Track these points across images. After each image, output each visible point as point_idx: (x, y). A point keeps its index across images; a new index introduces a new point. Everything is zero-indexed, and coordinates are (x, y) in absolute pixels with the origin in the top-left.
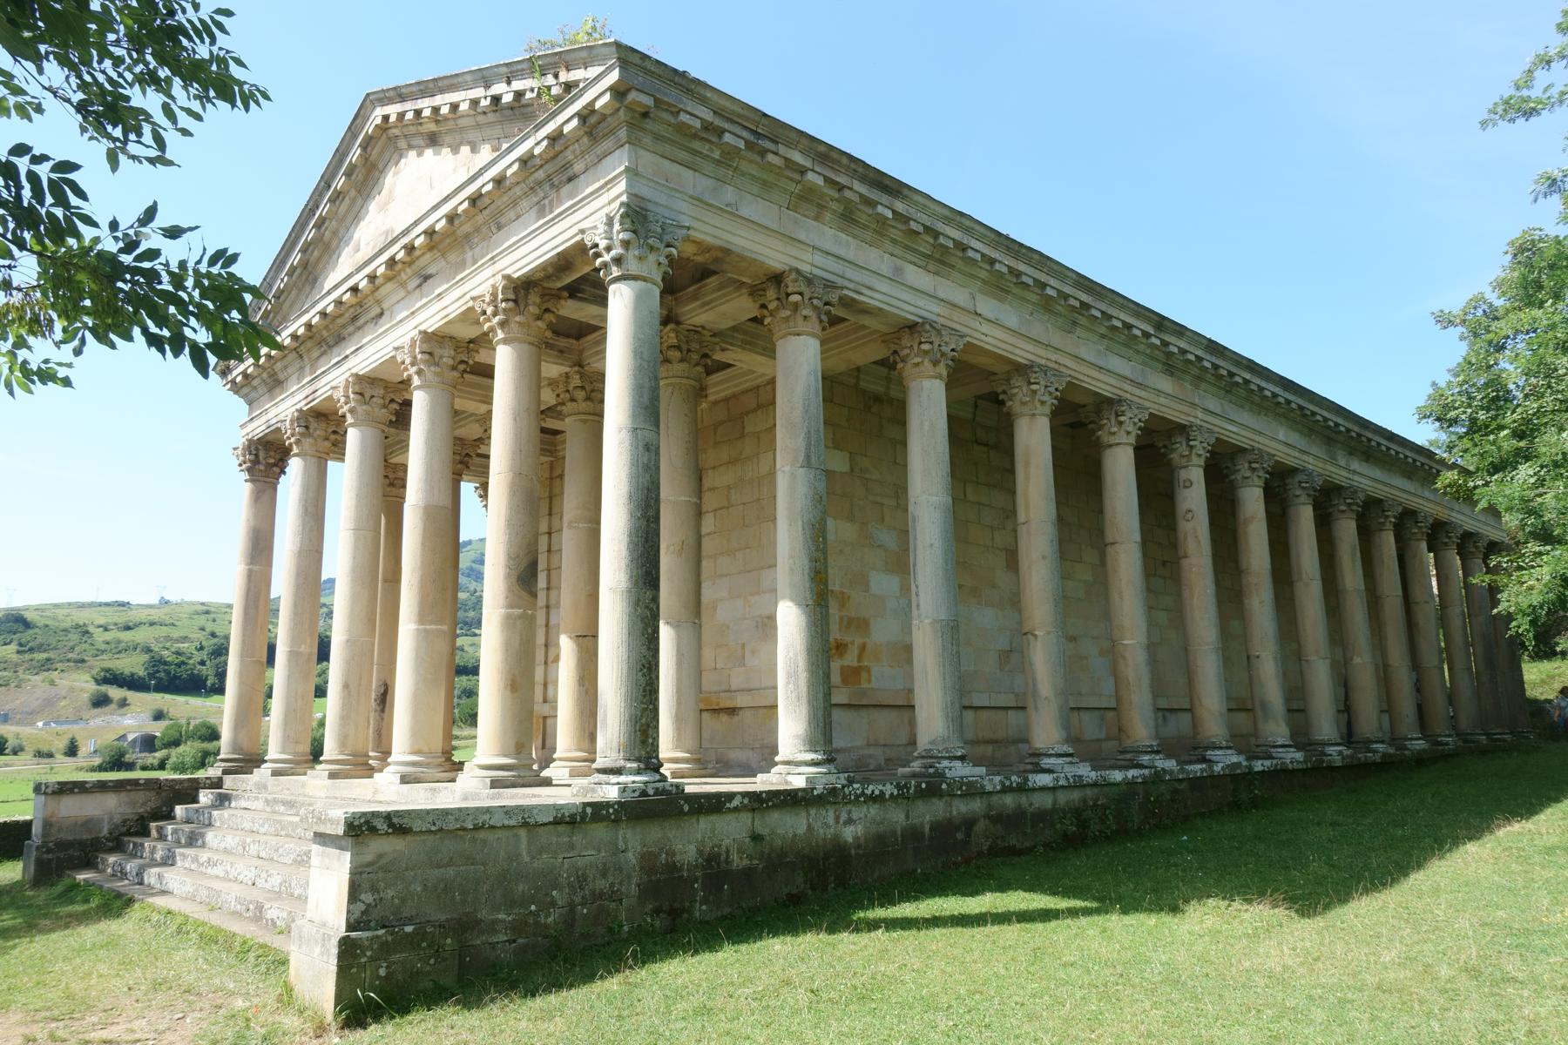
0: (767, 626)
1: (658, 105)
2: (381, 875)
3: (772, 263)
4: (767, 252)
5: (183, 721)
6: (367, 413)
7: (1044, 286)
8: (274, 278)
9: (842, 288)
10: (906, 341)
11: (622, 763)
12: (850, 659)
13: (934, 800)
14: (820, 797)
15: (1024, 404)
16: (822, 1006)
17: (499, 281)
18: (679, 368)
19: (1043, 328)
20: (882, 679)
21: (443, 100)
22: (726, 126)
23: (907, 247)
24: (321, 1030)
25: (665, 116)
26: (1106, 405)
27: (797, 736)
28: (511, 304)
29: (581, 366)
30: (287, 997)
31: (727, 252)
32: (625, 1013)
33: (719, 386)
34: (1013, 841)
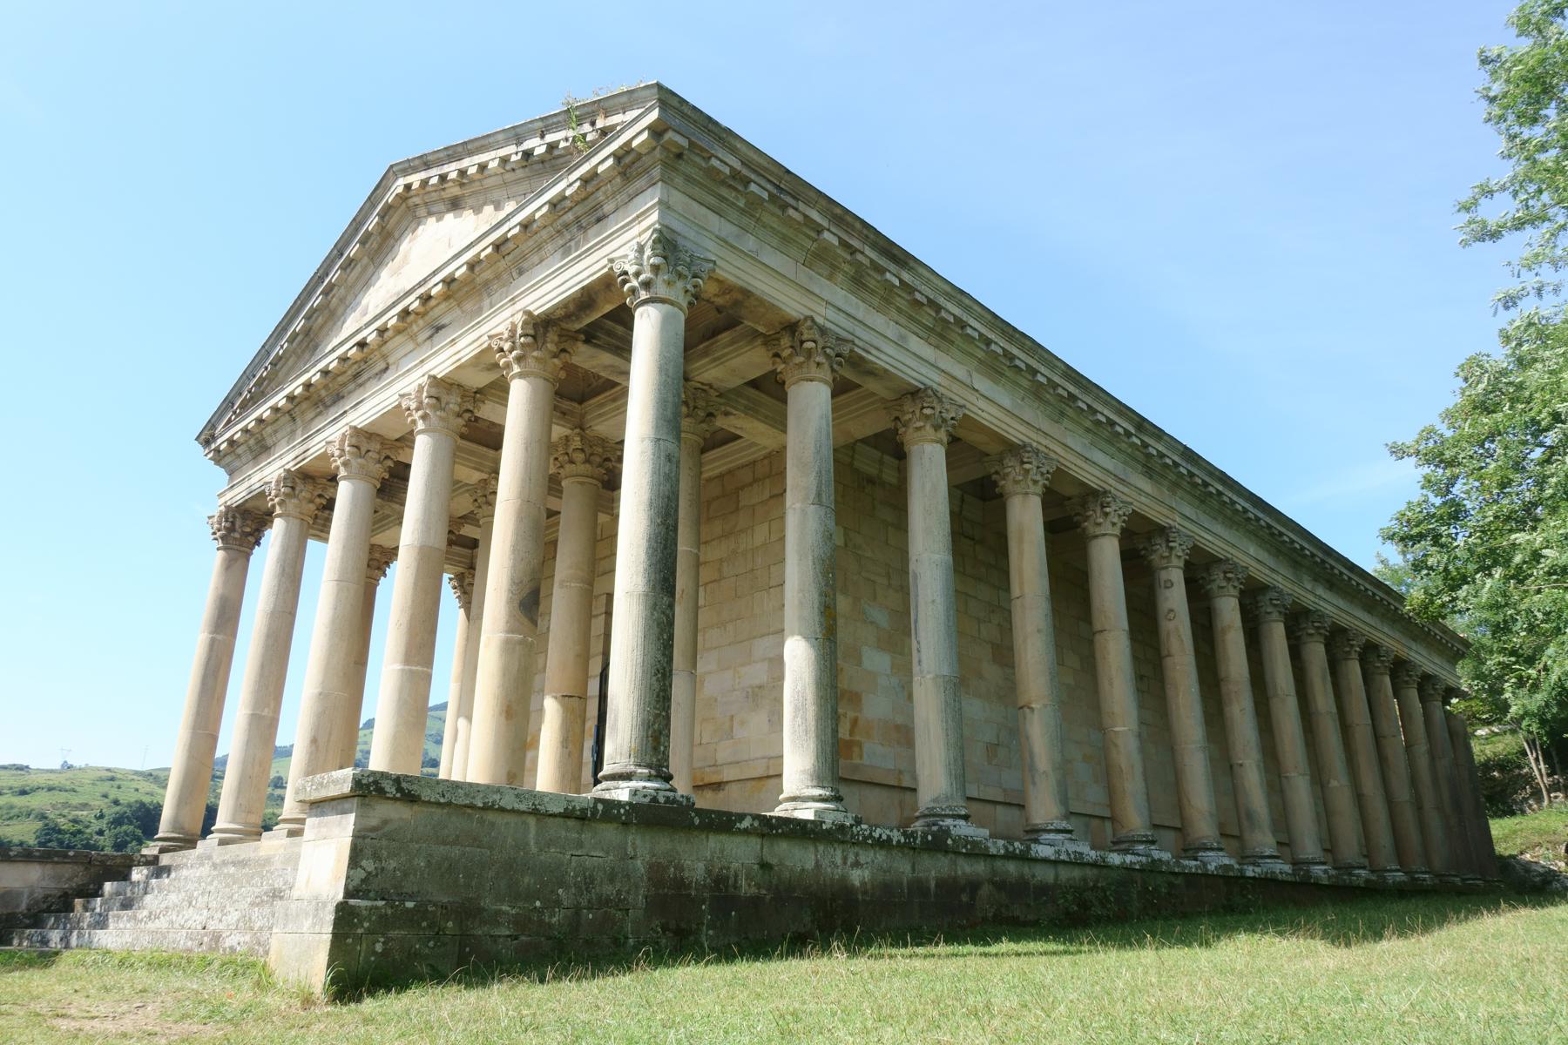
1: (690, 149)
2: (384, 842)
6: (362, 467)
7: (1035, 372)
8: (273, 346)
10: (908, 407)
14: (828, 831)
15: (1016, 482)
17: (519, 319)
21: (470, 164)
22: (753, 177)
23: (910, 318)
25: (698, 160)
26: (1092, 496)
27: (804, 772)
28: (529, 340)
29: (583, 429)
31: (747, 293)
34: (1017, 911)
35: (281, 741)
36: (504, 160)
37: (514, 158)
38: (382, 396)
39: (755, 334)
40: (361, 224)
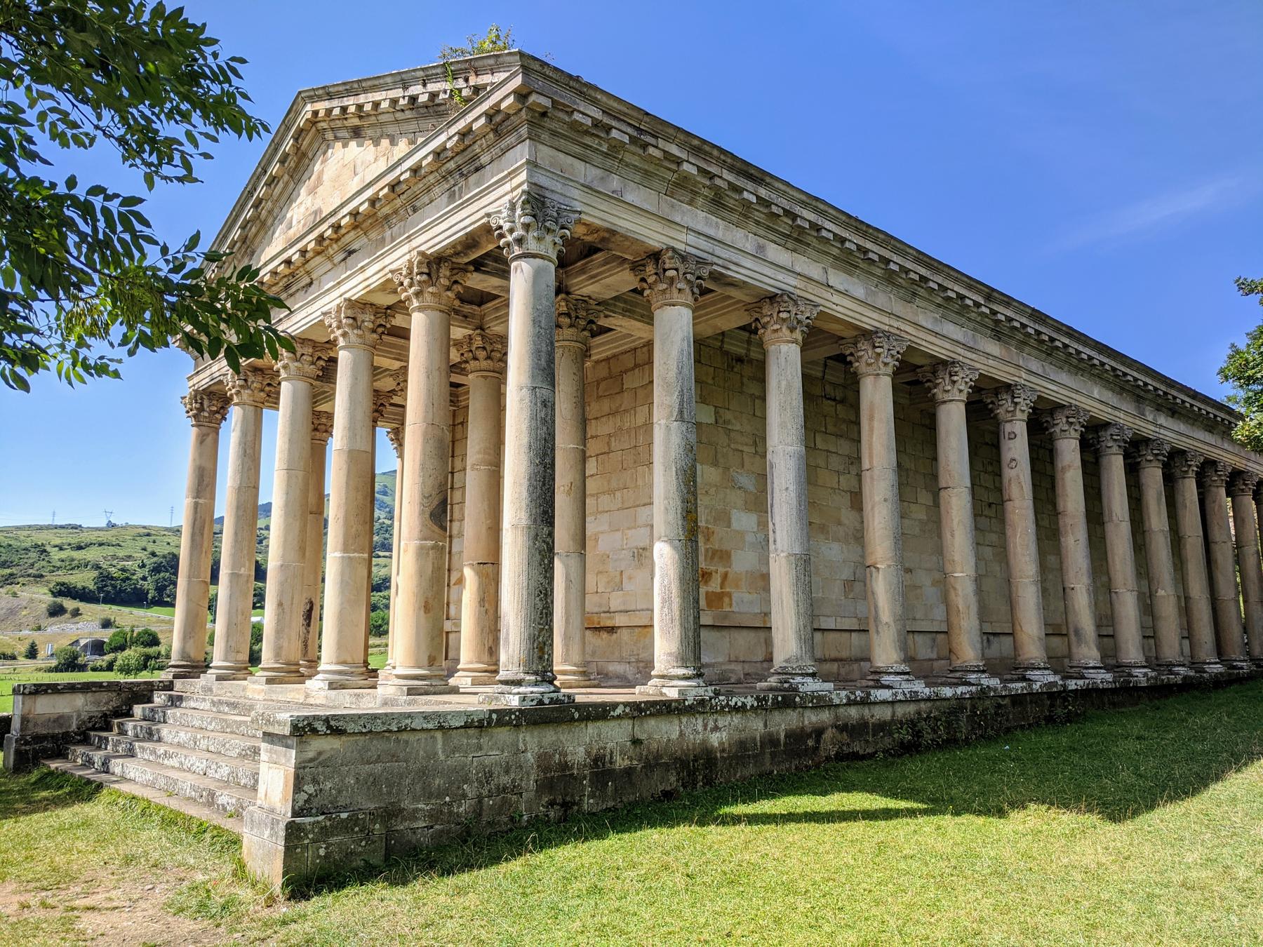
0: (643, 555)
1: (555, 107)
2: (320, 769)
3: (651, 242)
5: (128, 629)
6: (299, 369)
7: (888, 261)
9: (712, 264)
10: (766, 310)
11: (522, 676)
12: (714, 586)
13: (789, 711)
16: (697, 888)
18: (568, 332)
19: (883, 298)
20: (742, 603)
21: (366, 99)
22: (614, 123)
23: (769, 228)
24: (271, 901)
26: (940, 365)
27: (670, 654)
28: (425, 277)
29: (483, 329)
30: (240, 872)
31: (613, 233)
32: (528, 891)
33: (602, 348)
34: (857, 747)
38: (309, 310)
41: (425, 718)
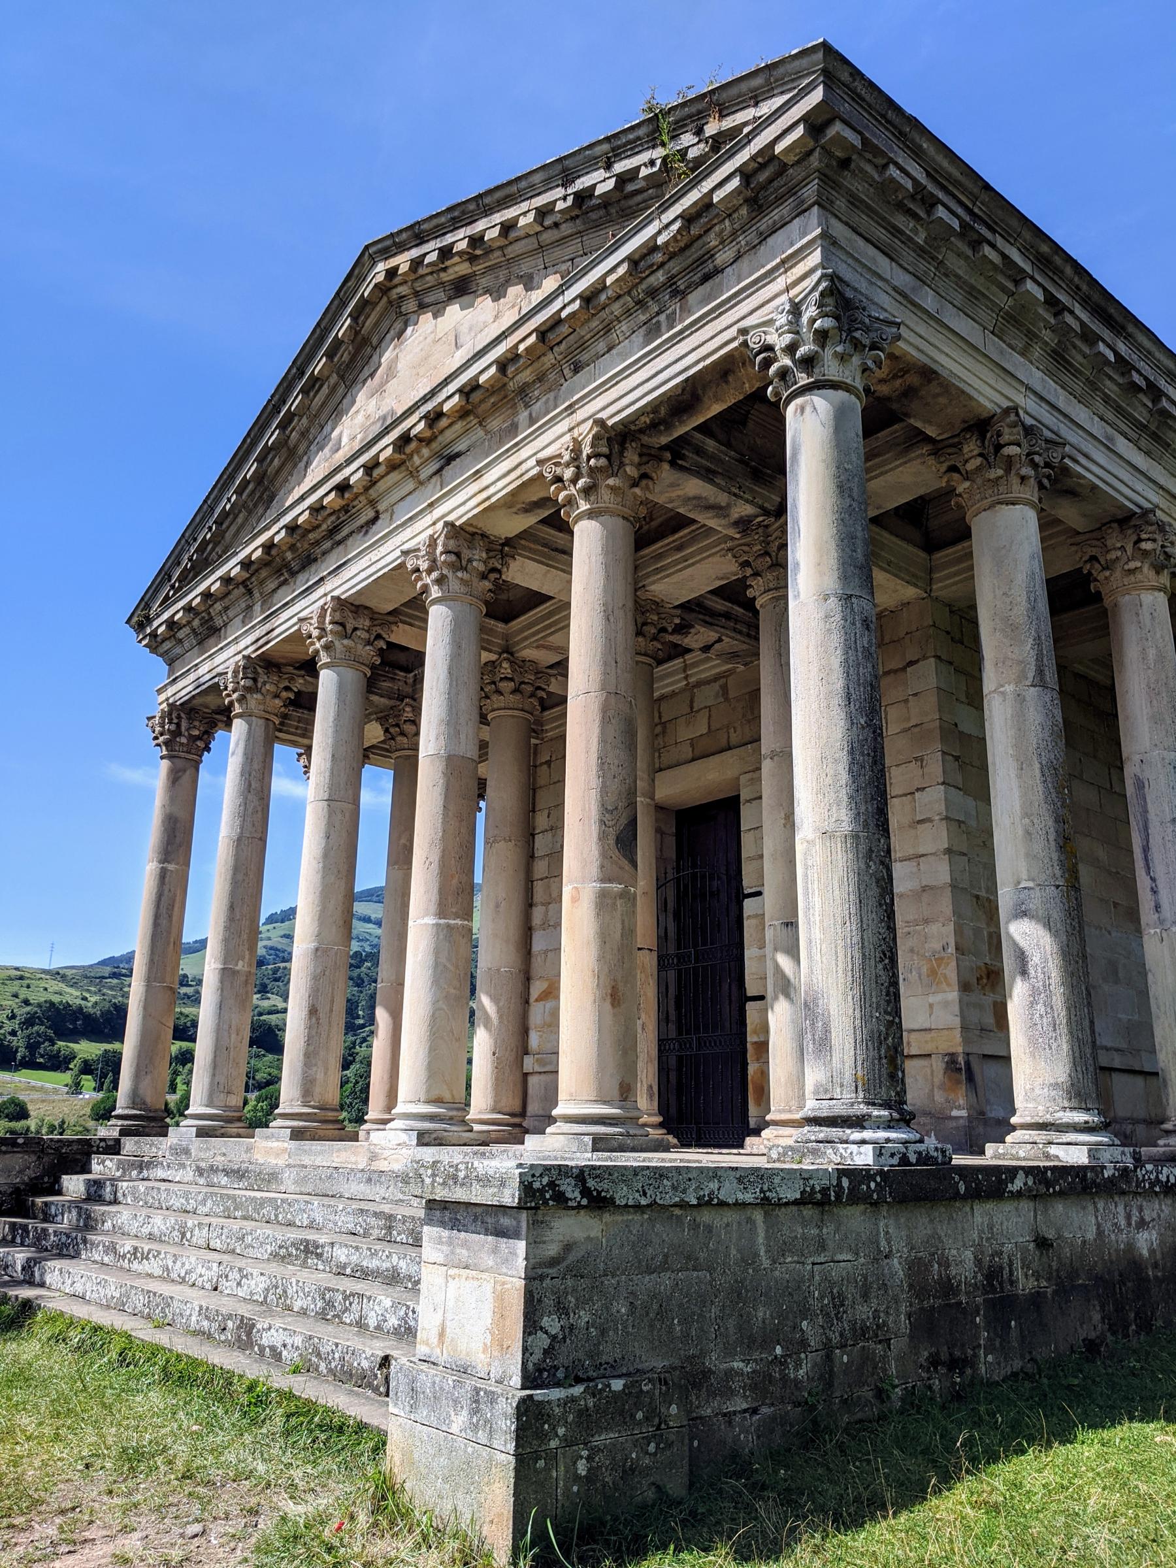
3: (981, 400)
4: (977, 383)
6: (349, 649)
8: (218, 500)
10: (1114, 540)
11: (863, 1109)
14: (1111, 1180)
17: (586, 432)
21: (488, 226)
22: (941, 195)
23: (1119, 410)
25: (869, 168)
28: (603, 462)
35: (189, 936)
36: (542, 213)
37: (560, 206)
38: (374, 556)
39: (920, 438)
40: (328, 330)
41: (740, 1180)
